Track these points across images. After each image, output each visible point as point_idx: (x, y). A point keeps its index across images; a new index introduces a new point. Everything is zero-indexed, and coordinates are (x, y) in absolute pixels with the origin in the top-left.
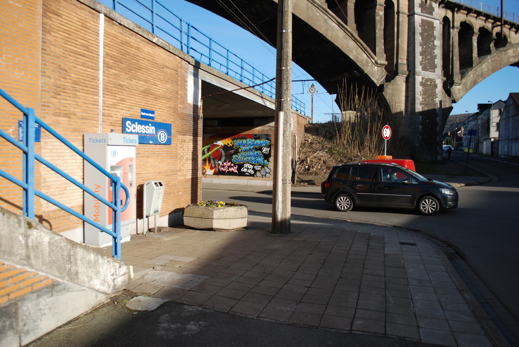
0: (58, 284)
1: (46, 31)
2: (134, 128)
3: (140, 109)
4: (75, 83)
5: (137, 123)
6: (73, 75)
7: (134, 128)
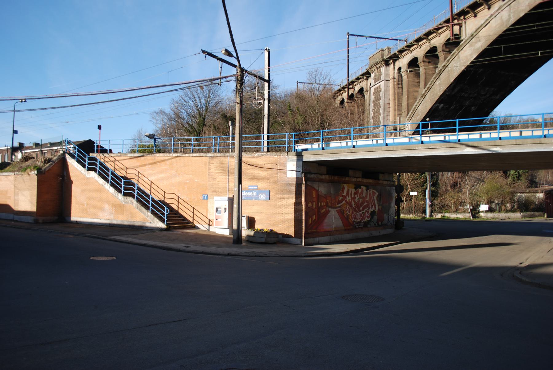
1: (209, 169)
4: (219, 182)
6: (218, 180)
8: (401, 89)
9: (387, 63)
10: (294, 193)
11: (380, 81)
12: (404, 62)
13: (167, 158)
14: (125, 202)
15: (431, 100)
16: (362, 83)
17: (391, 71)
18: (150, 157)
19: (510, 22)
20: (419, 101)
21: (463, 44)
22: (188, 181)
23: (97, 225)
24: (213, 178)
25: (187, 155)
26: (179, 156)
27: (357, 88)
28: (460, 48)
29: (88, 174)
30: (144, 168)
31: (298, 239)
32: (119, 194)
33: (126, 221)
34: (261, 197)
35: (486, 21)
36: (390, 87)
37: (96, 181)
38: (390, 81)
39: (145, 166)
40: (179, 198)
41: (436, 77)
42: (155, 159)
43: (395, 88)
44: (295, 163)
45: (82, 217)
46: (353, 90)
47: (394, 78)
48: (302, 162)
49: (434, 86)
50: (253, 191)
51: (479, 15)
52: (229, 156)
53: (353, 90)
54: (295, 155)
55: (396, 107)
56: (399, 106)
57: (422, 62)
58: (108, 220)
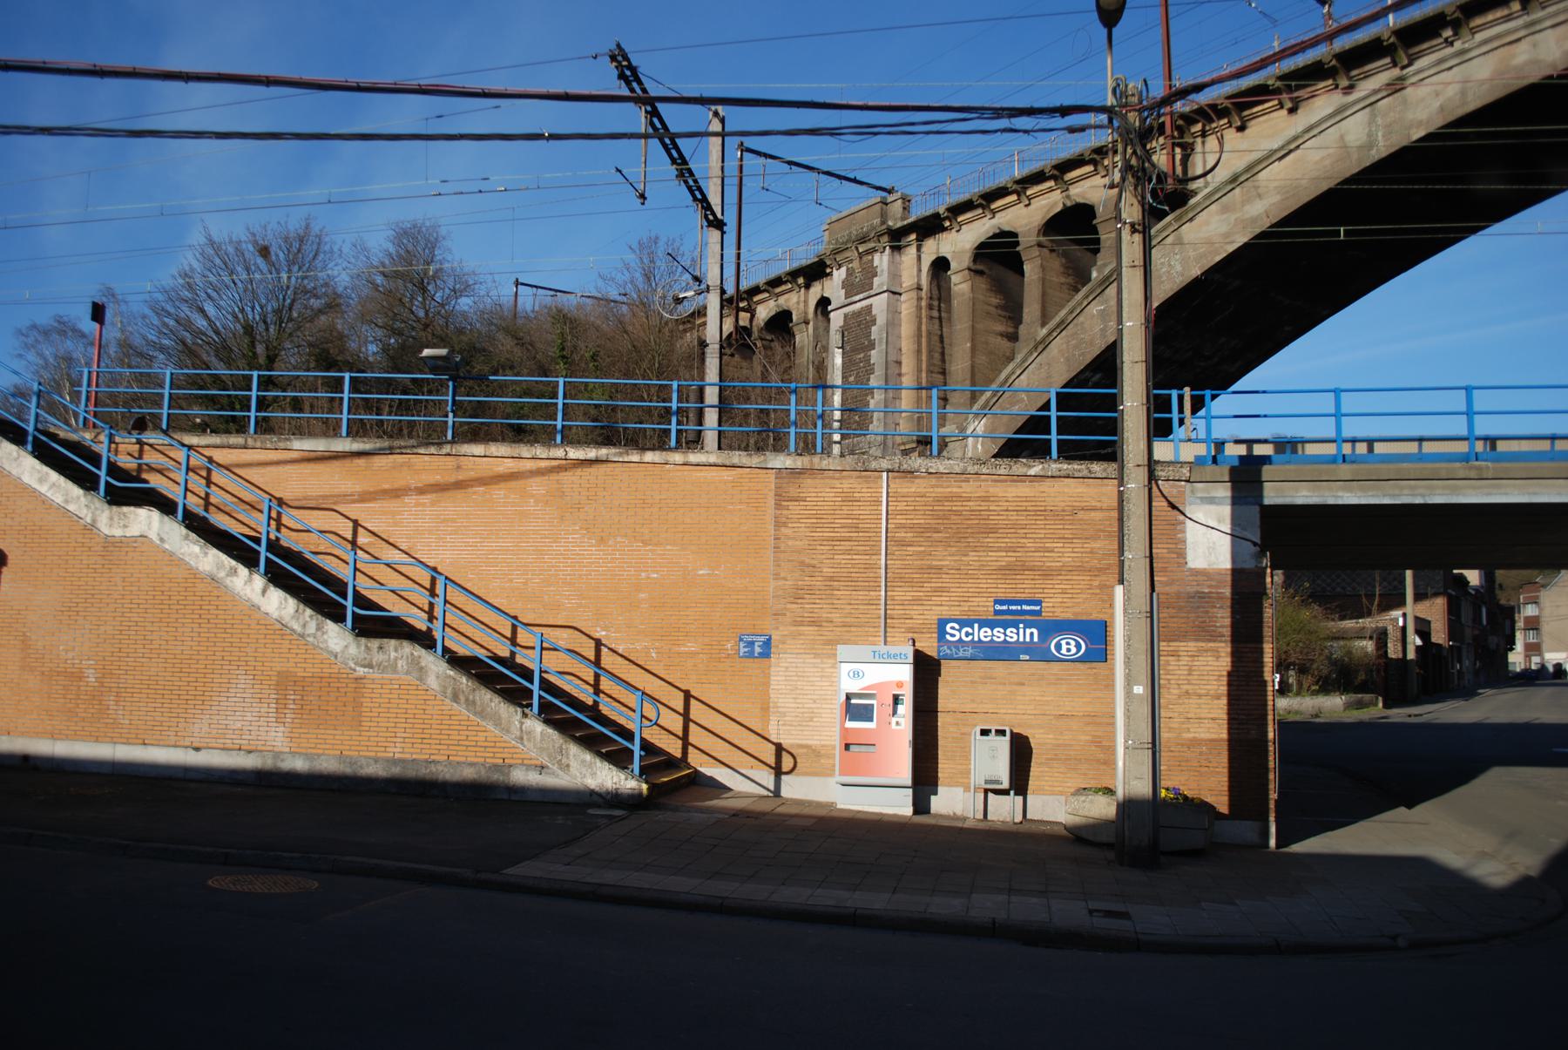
0: (547, 767)
1: (779, 524)
2: (967, 634)
3: (992, 599)
4: (831, 579)
5: (976, 626)
7: (967, 634)
8: (937, 321)
9: (896, 238)
10: (1227, 632)
11: (872, 292)
12: (959, 243)
13: (530, 465)
14: (370, 666)
15: (1068, 360)
16: (786, 296)
17: (912, 264)
18: (426, 458)
19: (1373, 152)
20: (1024, 360)
21: (1198, 204)
22: (657, 572)
23: (170, 779)
24: (802, 563)
25: (649, 456)
26: (607, 461)
27: (764, 312)
28: (1186, 212)
29: (111, 519)
30: (391, 505)
31: (1248, 823)
32: (331, 626)
33: (376, 760)
34: (1064, 647)
35: (1289, 143)
36: (904, 313)
37: (173, 559)
38: (903, 298)
39: (398, 496)
40: (604, 650)
41: (1091, 292)
42: (459, 467)
43: (919, 318)
44: (1226, 510)
45: (67, 738)
46: (749, 315)
47: (919, 288)
48: (1257, 508)
49: (1081, 318)
50: (1021, 621)
51: (1254, 128)
52: (888, 471)
53: (749, 315)
54: (1227, 479)
55: (924, 375)
56: (932, 372)
57: (1036, 248)
58: (250, 752)
